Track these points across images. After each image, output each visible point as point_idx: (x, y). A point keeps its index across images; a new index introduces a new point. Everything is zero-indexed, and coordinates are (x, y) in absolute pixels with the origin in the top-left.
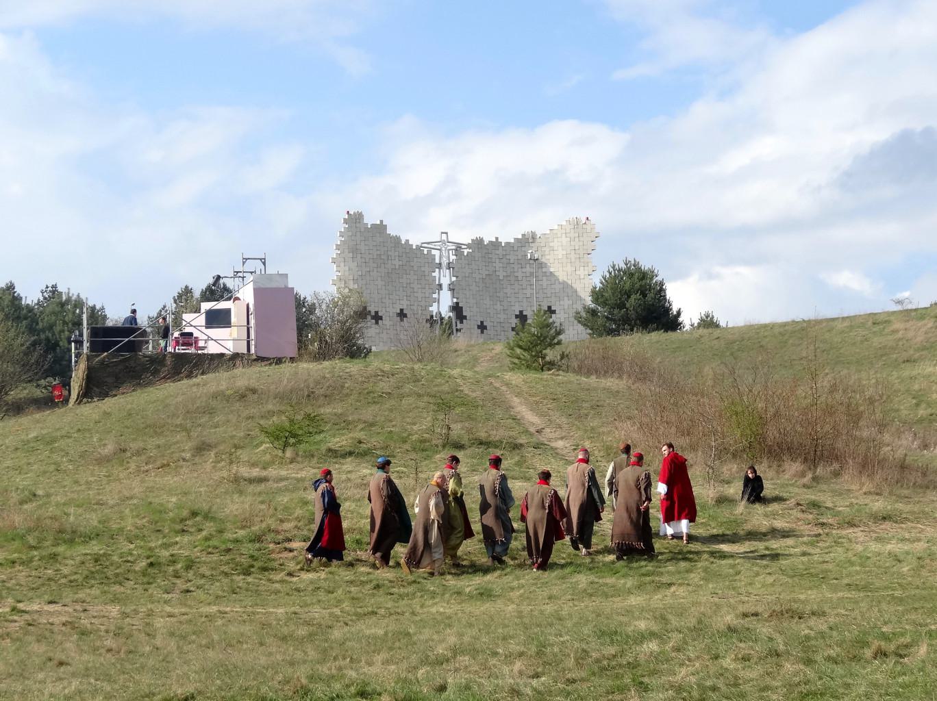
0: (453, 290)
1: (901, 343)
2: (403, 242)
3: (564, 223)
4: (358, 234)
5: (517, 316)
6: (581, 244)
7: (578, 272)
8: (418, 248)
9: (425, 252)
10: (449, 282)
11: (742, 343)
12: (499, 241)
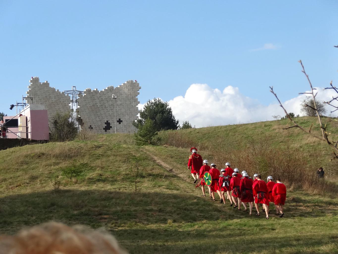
0: (78, 111)
1: (278, 134)
2: (56, 91)
3: (126, 83)
4: (37, 87)
5: (105, 123)
6: (133, 91)
7: (132, 104)
8: (63, 93)
9: (66, 95)
10: (76, 108)
11: (209, 134)
12: (98, 90)
